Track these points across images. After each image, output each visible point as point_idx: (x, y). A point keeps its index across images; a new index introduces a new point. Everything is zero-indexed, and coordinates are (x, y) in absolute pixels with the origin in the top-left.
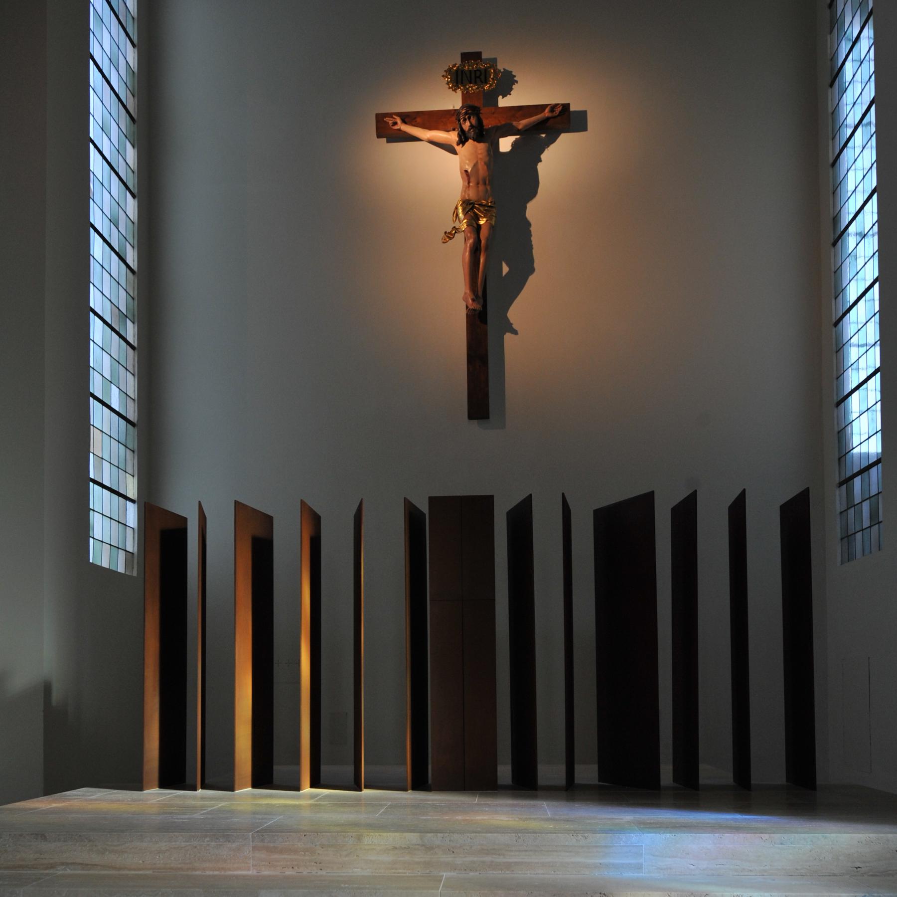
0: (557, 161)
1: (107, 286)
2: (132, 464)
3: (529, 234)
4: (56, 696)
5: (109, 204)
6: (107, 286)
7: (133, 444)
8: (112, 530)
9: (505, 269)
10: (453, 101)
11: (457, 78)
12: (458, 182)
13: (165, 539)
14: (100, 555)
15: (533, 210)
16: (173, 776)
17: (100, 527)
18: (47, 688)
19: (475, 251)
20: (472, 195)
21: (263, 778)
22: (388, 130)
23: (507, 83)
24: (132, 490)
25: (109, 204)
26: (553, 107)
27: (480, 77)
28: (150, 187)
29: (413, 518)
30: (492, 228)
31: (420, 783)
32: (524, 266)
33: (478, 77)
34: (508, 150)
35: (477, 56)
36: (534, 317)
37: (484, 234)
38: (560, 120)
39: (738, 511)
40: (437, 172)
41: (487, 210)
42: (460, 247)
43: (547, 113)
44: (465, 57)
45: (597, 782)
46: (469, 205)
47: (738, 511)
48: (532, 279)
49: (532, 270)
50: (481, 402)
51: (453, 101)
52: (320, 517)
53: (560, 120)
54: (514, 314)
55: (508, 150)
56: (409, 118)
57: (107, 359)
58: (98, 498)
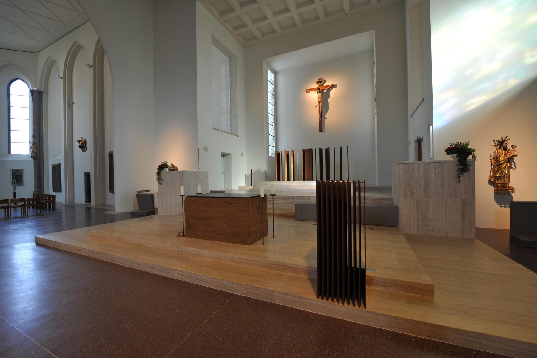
0: (333, 92)
1: (271, 119)
2: (274, 142)
5: (271, 108)
6: (271, 119)
8: (272, 152)
10: (317, 86)
11: (318, 83)
13: (278, 155)
14: (271, 155)
16: (279, 180)
17: (271, 151)
21: (288, 179)
22: (307, 91)
23: (325, 82)
24: (274, 145)
25: (271, 108)
27: (321, 82)
28: (276, 105)
31: (304, 180)
32: (328, 109)
33: (320, 82)
34: (324, 93)
35: (320, 79)
36: (329, 116)
38: (333, 86)
40: (314, 97)
42: (318, 107)
46: (319, 102)
50: (321, 130)
51: (317, 86)
52: (160, 166)
53: (333, 86)
55: (324, 93)
56: (310, 90)
57: (271, 130)
58: (270, 147)
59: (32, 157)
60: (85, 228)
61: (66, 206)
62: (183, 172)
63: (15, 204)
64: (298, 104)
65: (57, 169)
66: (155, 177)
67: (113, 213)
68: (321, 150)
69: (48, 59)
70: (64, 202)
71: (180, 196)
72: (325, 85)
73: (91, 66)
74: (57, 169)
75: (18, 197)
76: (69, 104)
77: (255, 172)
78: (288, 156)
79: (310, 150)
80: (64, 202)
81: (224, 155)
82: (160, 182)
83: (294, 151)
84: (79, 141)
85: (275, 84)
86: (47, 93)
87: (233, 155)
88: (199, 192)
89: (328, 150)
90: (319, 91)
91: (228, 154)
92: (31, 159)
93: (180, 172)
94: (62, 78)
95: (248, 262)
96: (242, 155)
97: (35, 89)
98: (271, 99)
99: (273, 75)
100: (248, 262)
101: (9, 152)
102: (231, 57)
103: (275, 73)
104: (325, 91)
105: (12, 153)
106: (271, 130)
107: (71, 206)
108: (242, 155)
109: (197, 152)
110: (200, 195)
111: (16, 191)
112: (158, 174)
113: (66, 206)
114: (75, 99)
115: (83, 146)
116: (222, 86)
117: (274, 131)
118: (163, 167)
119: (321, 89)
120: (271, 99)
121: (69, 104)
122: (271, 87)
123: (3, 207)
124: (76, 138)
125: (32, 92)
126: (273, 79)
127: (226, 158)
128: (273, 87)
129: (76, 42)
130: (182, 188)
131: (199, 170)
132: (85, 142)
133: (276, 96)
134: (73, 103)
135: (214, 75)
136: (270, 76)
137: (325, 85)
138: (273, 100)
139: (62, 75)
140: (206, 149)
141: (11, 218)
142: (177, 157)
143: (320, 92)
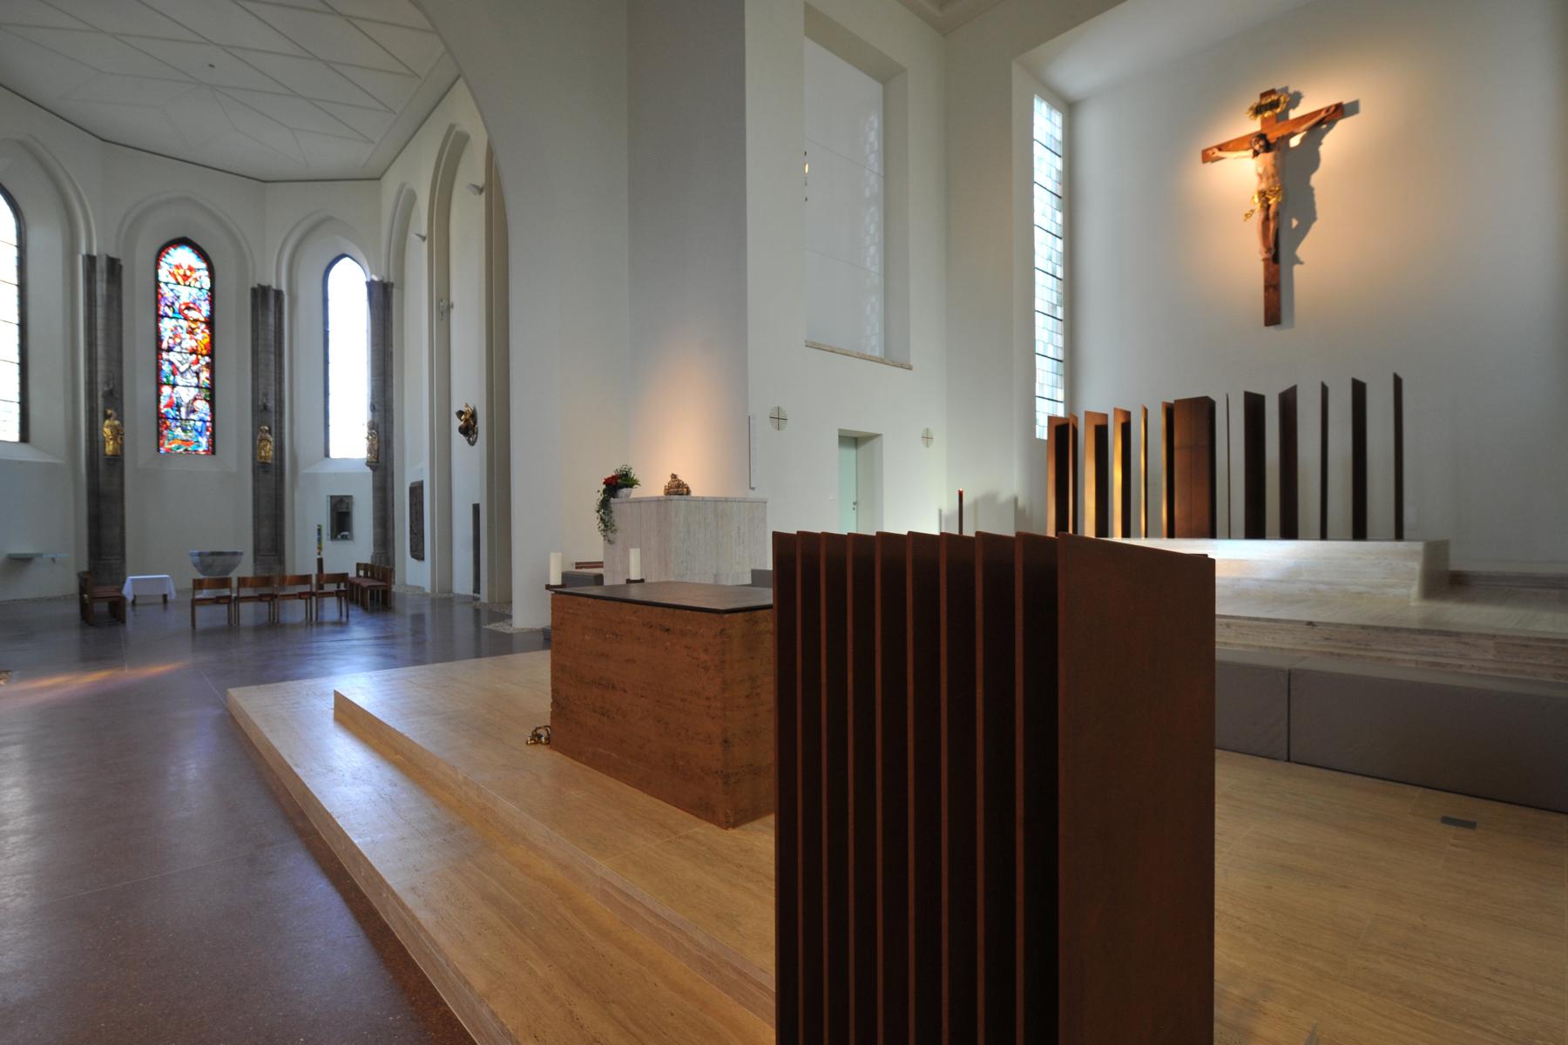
0: (1333, 143)
1: (1046, 292)
2: (1061, 381)
3: (1312, 195)
4: (1020, 503)
5: (1047, 250)
6: (1046, 292)
7: (1061, 371)
9: (1295, 223)
10: (1255, 126)
11: (1258, 110)
12: (1256, 179)
15: (1316, 180)
18: (1016, 500)
19: (1266, 219)
20: (1263, 186)
22: (1207, 157)
23: (1295, 100)
24: (1060, 395)
25: (1047, 250)
26: (1328, 109)
28: (1070, 234)
29: (1170, 411)
30: (1278, 204)
32: (1309, 217)
33: (1271, 104)
35: (1273, 92)
36: (1317, 257)
37: (1272, 210)
38: (1339, 111)
39: (1359, 390)
40: (1243, 175)
41: (1276, 193)
42: (1258, 217)
43: (1323, 114)
44: (1263, 95)
45: (456, 408)
46: (1262, 194)
47: (1359, 390)
48: (1315, 226)
49: (1314, 219)
50: (1273, 316)
52: (608, 482)
53: (1339, 111)
54: (1302, 251)
56: (1220, 148)
59: (369, 463)
60: (472, 662)
61: (433, 600)
62: (703, 500)
63: (321, 587)
64: (1167, 213)
65: (416, 491)
66: (594, 519)
67: (507, 630)
68: (1254, 405)
69: (400, 192)
70: (428, 590)
71: (548, 587)
72: (1293, 114)
73: (481, 191)
74: (416, 491)
75: (327, 570)
76: (442, 310)
77: (976, 503)
78: (1101, 433)
79: (1203, 410)
80: (428, 590)
81: (852, 440)
82: (610, 535)
83: (1127, 414)
84: (460, 413)
85: (1070, 151)
86: (402, 289)
87: (885, 437)
88: (634, 576)
89: (1288, 402)
90: (1263, 143)
91: (870, 437)
92: (368, 470)
93: (697, 499)
94: (424, 238)
95: (652, 920)
96: (927, 438)
97: (375, 278)
98: (1046, 213)
99: (1058, 118)
100: (652, 920)
101: (327, 455)
102: (885, 73)
103: (1069, 108)
104: (1295, 142)
105: (334, 454)
106: (1048, 337)
107: (444, 600)
108: (927, 438)
109: (747, 431)
110: (635, 593)
111: (324, 555)
112: (604, 504)
113: (433, 600)
114: (454, 298)
115: (468, 430)
116: (867, 193)
117: (1059, 340)
118: (618, 484)
119: (1272, 137)
120: (1046, 213)
121: (442, 310)
122: (1046, 168)
123: (300, 596)
124: (456, 408)
125: (370, 285)
126: (1058, 135)
127: (863, 449)
128: (1058, 163)
129: (452, 127)
130: (634, 556)
131: (752, 495)
132: (473, 415)
133: (1070, 199)
134: (449, 307)
135: (814, 144)
136: (1046, 123)
137: (1293, 114)
138: (1059, 217)
139: (424, 232)
140: (778, 419)
141: (320, 624)
142: (680, 450)
143: (1268, 148)
